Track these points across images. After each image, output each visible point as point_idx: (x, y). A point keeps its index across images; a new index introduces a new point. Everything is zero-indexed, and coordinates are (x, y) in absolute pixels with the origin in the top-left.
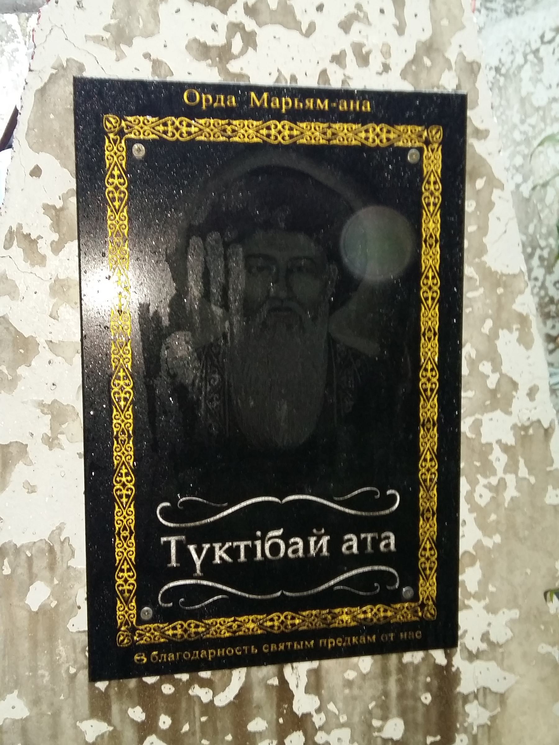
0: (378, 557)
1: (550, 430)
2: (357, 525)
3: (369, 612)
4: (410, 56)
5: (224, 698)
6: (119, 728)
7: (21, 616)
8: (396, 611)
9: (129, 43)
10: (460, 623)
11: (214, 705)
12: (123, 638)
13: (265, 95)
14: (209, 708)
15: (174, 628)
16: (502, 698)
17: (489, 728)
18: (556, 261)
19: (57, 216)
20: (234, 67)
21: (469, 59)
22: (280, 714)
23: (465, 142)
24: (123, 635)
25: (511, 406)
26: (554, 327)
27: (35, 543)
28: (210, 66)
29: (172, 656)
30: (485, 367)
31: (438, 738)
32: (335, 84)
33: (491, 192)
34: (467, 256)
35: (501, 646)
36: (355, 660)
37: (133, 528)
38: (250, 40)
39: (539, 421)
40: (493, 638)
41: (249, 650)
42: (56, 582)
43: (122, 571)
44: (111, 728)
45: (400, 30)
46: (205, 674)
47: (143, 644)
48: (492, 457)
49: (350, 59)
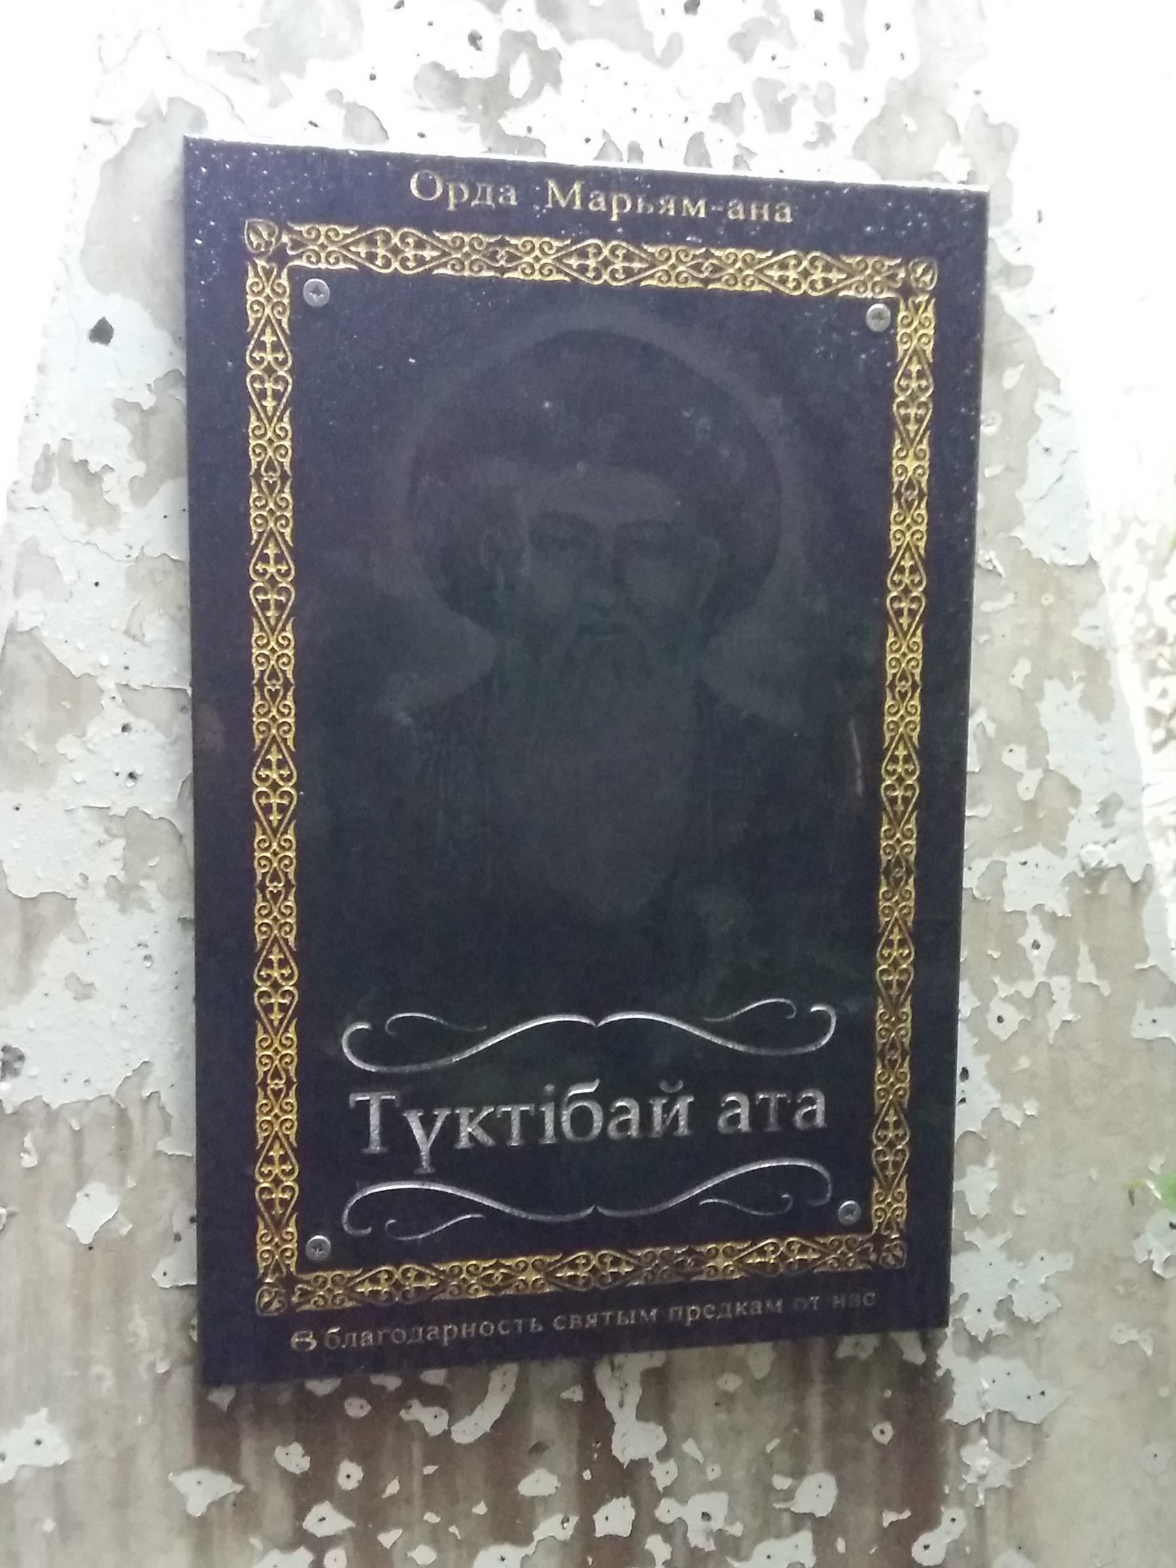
0: (790, 1140)
1: (1143, 887)
2: (746, 1076)
3: (768, 1252)
4: (873, 110)
5: (471, 1428)
6: (255, 1488)
7: (59, 1255)
8: (824, 1251)
9: (300, 72)
10: (953, 1278)
11: (452, 1441)
12: (268, 1299)
13: (577, 187)
14: (441, 1448)
15: (374, 1280)
16: (1036, 1432)
17: (1010, 1493)
18: (1171, 551)
19: (144, 424)
20: (513, 123)
21: (994, 119)
22: (584, 1463)
23: (981, 292)
24: (270, 1293)
25: (1064, 838)
26: (1164, 694)
27: (89, 1102)
28: (466, 119)
29: (368, 1338)
30: (1015, 758)
31: (907, 1514)
32: (721, 167)
33: (1035, 396)
34: (983, 525)
35: (1036, 1327)
36: (739, 1350)
37: (292, 1074)
38: (548, 70)
39: (1120, 868)
40: (1019, 1310)
41: (526, 1326)
42: (131, 1183)
43: (269, 1160)
44: (239, 1488)
45: (856, 54)
46: (434, 1376)
47: (309, 1312)
48: (1025, 941)
49: (753, 115)
